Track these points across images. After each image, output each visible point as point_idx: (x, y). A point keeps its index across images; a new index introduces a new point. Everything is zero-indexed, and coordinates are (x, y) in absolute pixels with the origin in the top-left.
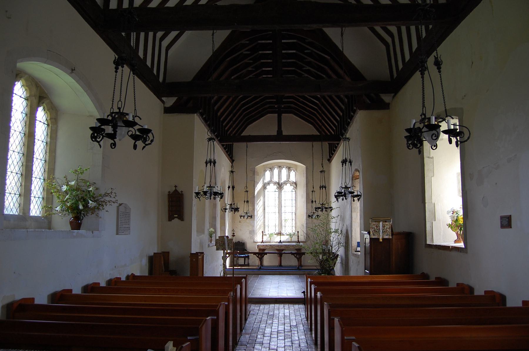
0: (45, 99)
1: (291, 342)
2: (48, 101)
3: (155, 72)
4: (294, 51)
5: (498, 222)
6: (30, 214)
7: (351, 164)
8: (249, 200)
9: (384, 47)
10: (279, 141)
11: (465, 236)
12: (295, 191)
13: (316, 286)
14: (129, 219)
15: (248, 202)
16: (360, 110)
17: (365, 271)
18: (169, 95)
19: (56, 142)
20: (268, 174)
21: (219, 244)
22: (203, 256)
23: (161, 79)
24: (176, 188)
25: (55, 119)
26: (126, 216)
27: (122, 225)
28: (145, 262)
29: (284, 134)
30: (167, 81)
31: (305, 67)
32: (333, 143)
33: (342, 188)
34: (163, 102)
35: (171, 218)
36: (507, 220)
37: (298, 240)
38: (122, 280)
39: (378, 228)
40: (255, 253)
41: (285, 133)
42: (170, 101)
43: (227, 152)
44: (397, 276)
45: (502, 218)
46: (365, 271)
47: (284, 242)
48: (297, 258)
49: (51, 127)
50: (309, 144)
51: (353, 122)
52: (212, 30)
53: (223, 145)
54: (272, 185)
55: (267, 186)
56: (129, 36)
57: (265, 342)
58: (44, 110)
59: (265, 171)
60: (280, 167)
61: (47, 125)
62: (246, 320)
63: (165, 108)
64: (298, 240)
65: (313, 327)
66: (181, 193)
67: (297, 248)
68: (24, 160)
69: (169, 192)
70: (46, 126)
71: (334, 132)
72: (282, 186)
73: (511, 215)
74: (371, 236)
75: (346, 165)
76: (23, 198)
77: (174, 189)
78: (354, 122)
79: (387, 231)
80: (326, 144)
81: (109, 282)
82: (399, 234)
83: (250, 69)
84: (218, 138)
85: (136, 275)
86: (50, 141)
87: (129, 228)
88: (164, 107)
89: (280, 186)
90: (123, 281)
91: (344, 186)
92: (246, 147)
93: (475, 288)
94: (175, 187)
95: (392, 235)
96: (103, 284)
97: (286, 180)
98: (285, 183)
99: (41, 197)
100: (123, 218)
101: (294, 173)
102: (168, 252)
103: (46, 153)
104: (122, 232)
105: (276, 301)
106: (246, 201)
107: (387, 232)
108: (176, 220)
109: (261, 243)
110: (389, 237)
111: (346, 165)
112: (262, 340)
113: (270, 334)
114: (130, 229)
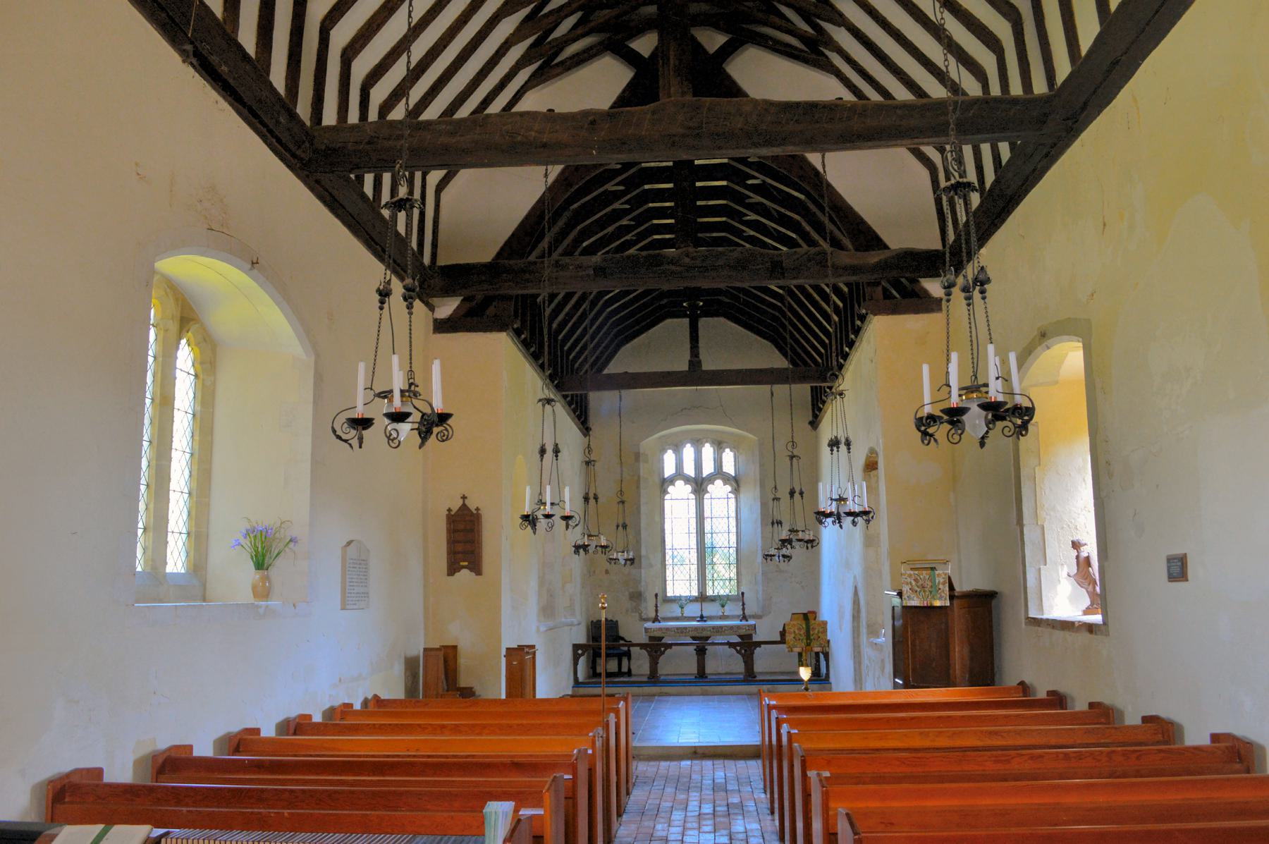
0: (191, 323)
1: (729, 837)
2: (197, 325)
4: (724, 183)
6: (136, 568)
7: (849, 449)
8: (627, 522)
9: (924, 174)
11: (1100, 601)
12: (736, 498)
13: (791, 728)
14: (365, 574)
15: (625, 526)
16: (875, 315)
18: (447, 292)
19: (213, 413)
20: (669, 459)
21: (793, 635)
22: (534, 658)
23: (427, 260)
24: (464, 501)
25: (211, 363)
26: (359, 568)
27: (352, 588)
28: (398, 670)
29: (705, 367)
30: (442, 261)
31: (748, 215)
32: (820, 386)
33: (831, 499)
35: (453, 569)
36: (1180, 564)
37: (744, 613)
38: (354, 708)
39: (918, 584)
40: (642, 646)
42: (447, 307)
43: (574, 411)
44: (966, 690)
45: (1170, 560)
46: (894, 680)
47: (711, 618)
49: (203, 380)
51: (861, 340)
52: (544, 165)
54: (680, 483)
55: (668, 487)
56: (360, 180)
57: (671, 837)
58: (189, 345)
59: (664, 451)
60: (698, 444)
61: (193, 377)
62: (628, 793)
63: (435, 320)
64: (744, 613)
65: (776, 805)
66: (475, 512)
67: (743, 632)
68: (151, 454)
69: (449, 510)
70: (192, 378)
71: (821, 358)
72: (703, 487)
73: (1186, 554)
74: (904, 602)
75: (838, 451)
76: (151, 534)
77: (460, 502)
78: (865, 339)
79: (940, 589)
81: (330, 713)
83: (624, 223)
84: (553, 382)
85: (382, 698)
86: (201, 411)
88: (433, 318)
89: (699, 485)
90: (357, 711)
92: (619, 399)
93: (1126, 713)
94: (462, 498)
95: (952, 598)
96: (317, 718)
97: (713, 471)
98: (711, 479)
99: (184, 531)
100: (354, 573)
101: (732, 454)
102: (455, 647)
103: (192, 436)
104: (354, 602)
105: (695, 753)
106: (621, 523)
107: (940, 591)
108: (465, 572)
109: (654, 622)
110: (945, 603)
111: (838, 451)
112: (664, 834)
113: (683, 822)
114: (368, 597)
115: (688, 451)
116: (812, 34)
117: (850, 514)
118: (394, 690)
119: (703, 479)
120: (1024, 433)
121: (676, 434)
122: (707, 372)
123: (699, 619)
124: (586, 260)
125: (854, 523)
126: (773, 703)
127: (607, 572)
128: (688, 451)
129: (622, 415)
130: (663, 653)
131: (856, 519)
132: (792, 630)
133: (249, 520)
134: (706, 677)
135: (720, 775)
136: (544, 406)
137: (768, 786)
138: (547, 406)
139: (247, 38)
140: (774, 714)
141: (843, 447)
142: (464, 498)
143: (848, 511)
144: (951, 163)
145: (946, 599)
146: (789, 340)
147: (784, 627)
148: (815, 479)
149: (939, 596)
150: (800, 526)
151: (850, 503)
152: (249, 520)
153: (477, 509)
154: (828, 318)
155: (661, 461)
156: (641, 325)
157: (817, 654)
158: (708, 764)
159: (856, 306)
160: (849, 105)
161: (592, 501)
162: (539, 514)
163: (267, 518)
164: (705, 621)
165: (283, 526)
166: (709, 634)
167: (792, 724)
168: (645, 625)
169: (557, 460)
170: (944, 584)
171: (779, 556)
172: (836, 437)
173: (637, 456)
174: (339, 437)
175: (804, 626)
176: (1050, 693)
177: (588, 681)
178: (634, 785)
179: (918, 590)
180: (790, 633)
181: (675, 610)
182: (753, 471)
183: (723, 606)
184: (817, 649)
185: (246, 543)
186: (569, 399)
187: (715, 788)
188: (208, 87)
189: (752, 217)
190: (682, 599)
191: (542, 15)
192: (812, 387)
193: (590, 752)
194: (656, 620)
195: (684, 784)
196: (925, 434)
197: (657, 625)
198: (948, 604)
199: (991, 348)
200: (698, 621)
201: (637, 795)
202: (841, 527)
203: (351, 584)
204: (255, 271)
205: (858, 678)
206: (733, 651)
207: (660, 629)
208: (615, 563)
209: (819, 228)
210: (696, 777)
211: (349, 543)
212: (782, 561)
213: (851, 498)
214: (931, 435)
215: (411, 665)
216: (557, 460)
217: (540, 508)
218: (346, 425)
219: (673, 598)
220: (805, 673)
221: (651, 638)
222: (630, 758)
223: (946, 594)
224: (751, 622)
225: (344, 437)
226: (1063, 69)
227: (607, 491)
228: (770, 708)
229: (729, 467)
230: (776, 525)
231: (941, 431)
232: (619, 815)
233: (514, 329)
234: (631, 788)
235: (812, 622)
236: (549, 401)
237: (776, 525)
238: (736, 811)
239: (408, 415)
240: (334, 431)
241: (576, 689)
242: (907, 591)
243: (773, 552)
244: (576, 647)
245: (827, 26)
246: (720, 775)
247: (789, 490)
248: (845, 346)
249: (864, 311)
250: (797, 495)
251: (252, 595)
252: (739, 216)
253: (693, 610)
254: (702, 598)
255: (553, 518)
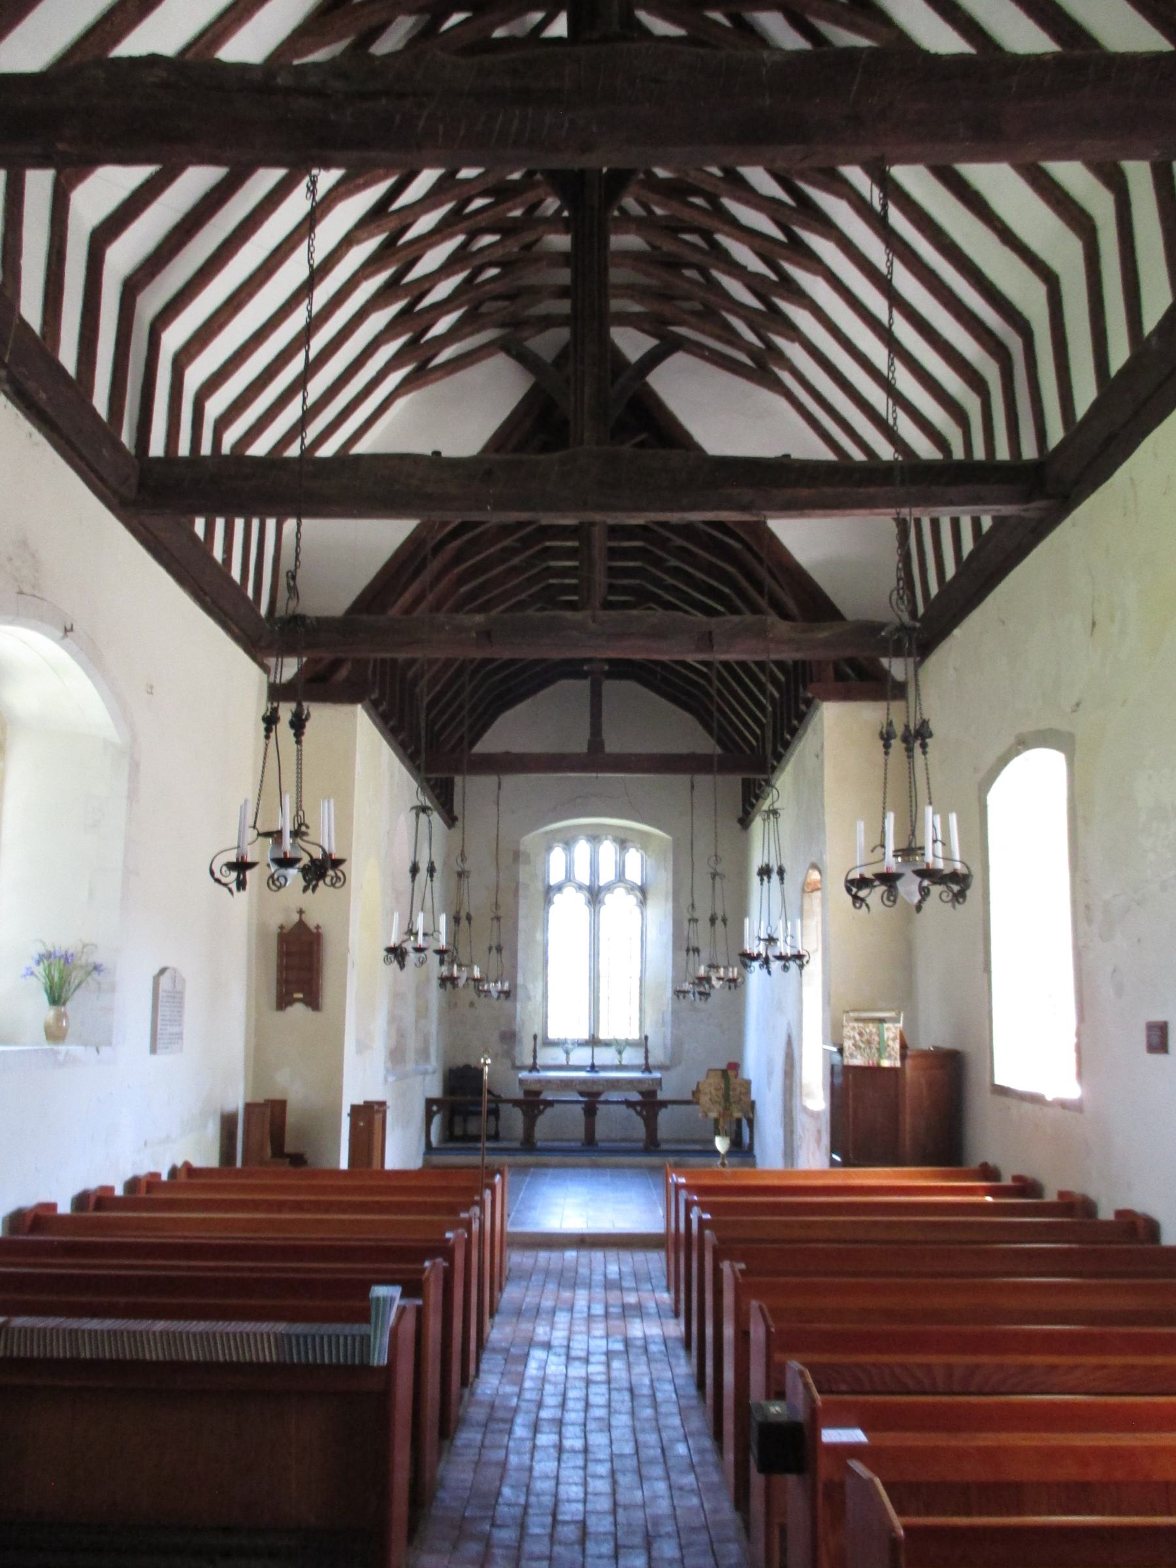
3: (250, 593)
5: (1141, 1038)
10: (592, 771)
15: (499, 949)
17: (831, 1156)
18: (288, 650)
20: (557, 857)
23: (263, 610)
28: (212, 1131)
32: (755, 779)
33: (760, 939)
34: (265, 669)
35: (283, 1001)
37: (647, 1063)
40: (516, 1103)
41: (613, 745)
42: (290, 668)
46: (831, 1156)
47: (605, 1068)
48: (642, 1117)
50: (682, 780)
53: (428, 780)
57: (555, 1342)
59: (549, 849)
60: (595, 838)
64: (647, 1063)
66: (314, 931)
67: (645, 1087)
69: (282, 927)
72: (601, 896)
75: (769, 882)
77: (295, 918)
78: (810, 730)
80: (734, 782)
81: (133, 1185)
82: (924, 1055)
87: (180, 1036)
91: (764, 935)
95: (903, 1057)
106: (494, 944)
111: (769, 882)
112: (546, 1338)
115: (582, 848)
116: (757, 347)
117: (780, 957)
118: (206, 1157)
119: (600, 887)
120: (961, 900)
121: (569, 828)
122: (610, 755)
123: (588, 1069)
124: (463, 619)
125: (785, 968)
126: (682, 1180)
127: (472, 1004)
128: (582, 848)
129: (500, 803)
130: (541, 1112)
131: (787, 964)
132: (707, 1091)
133: (44, 944)
134: (597, 1145)
135: (613, 1269)
136: (417, 815)
137: (673, 1284)
138: (422, 816)
139: (68, 357)
140: (683, 1195)
141: (775, 877)
142: (301, 912)
143: (778, 954)
144: (897, 603)
145: (895, 1059)
146: (716, 714)
147: (698, 1086)
148: (742, 910)
149: (887, 1054)
150: (721, 960)
151: (780, 944)
152: (44, 944)
153: (318, 927)
154: (762, 709)
155: (546, 862)
156: (720, 1218)
157: (739, 1121)
158: (598, 1255)
159: (801, 689)
160: (797, 465)
161: (464, 922)
162: (409, 946)
163: (64, 941)
164: (597, 1072)
165: (85, 950)
166: (601, 1088)
167: (704, 1207)
168: (520, 1075)
169: (432, 880)
170: (894, 1039)
171: (694, 994)
172: (768, 865)
173: (516, 855)
174: (218, 881)
175: (723, 1086)
176: (1016, 1178)
177: (444, 1146)
178: (507, 1279)
179: (863, 1046)
180: (705, 1094)
181: (556, 1056)
182: (663, 881)
183: (620, 1053)
184: (737, 1115)
185: (40, 970)
186: (432, 783)
187: (608, 1285)
188: (21, 417)
189: (674, 562)
190: (569, 1042)
191: (421, 310)
192: (743, 780)
193: (466, 1236)
194: (534, 1068)
195: (569, 1280)
196: (855, 898)
197: (535, 1075)
198: (898, 1064)
199: (929, 810)
200: (588, 1071)
201: (511, 1294)
202: (769, 973)
203: (164, 1023)
204: (68, 640)
205: (790, 1152)
206: (631, 1112)
207: (539, 1081)
208: (485, 996)
209: (758, 586)
210: (583, 1271)
211: (163, 971)
212: (698, 1000)
213: (781, 938)
214: (863, 900)
215: (228, 1123)
216: (432, 880)
217: (410, 938)
218: (225, 869)
219: (556, 1041)
220: (721, 1144)
221: (527, 1093)
222: (505, 1245)
223: (896, 1053)
224: (657, 1075)
225: (224, 880)
226: (1056, 434)
227: (478, 899)
228: (678, 1187)
229: (634, 874)
230: (691, 953)
231: (874, 895)
232: (492, 1315)
233: (370, 700)
234: (503, 1283)
235: (732, 1080)
236: (424, 809)
237: (691, 953)
238: (633, 1313)
239: (297, 860)
240: (212, 873)
241: (427, 1156)
242: (849, 1048)
243: (687, 986)
244: (429, 1102)
245: (780, 342)
246: (613, 1269)
247: (709, 916)
248: (785, 731)
249: (810, 695)
250: (719, 922)
251: (44, 1036)
252: (658, 562)
253: (582, 1056)
254: (594, 1042)
255: (426, 952)
